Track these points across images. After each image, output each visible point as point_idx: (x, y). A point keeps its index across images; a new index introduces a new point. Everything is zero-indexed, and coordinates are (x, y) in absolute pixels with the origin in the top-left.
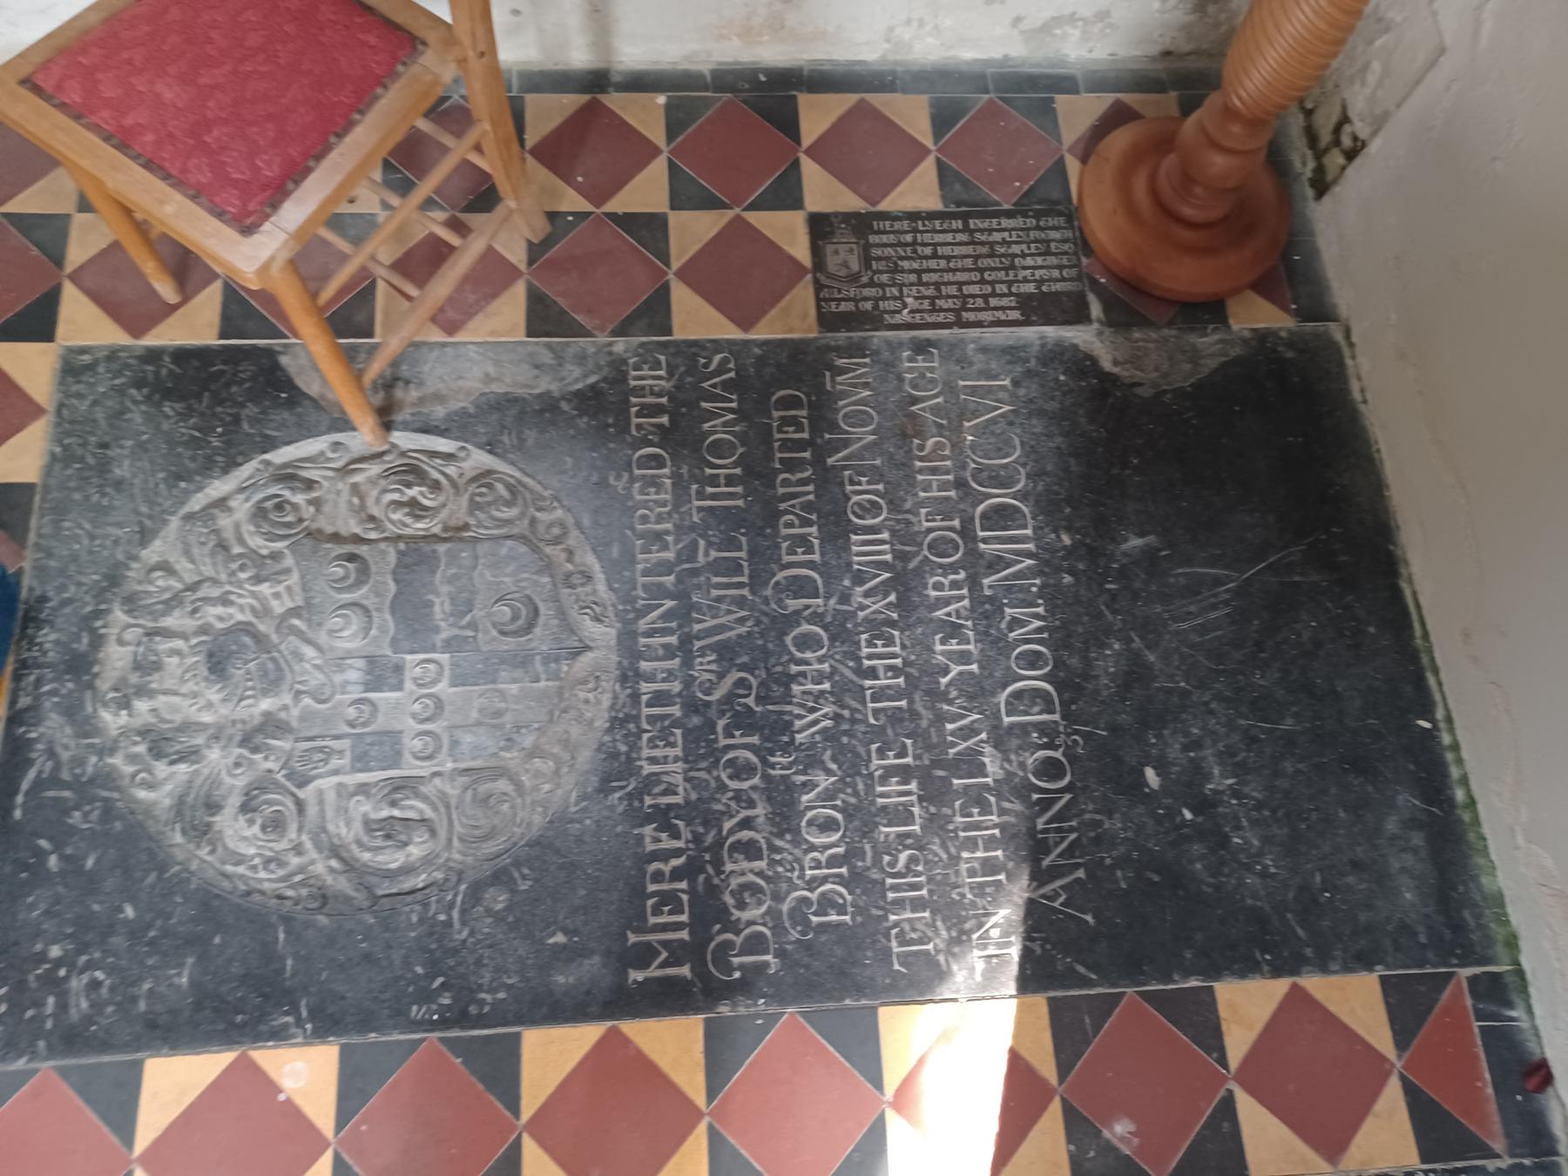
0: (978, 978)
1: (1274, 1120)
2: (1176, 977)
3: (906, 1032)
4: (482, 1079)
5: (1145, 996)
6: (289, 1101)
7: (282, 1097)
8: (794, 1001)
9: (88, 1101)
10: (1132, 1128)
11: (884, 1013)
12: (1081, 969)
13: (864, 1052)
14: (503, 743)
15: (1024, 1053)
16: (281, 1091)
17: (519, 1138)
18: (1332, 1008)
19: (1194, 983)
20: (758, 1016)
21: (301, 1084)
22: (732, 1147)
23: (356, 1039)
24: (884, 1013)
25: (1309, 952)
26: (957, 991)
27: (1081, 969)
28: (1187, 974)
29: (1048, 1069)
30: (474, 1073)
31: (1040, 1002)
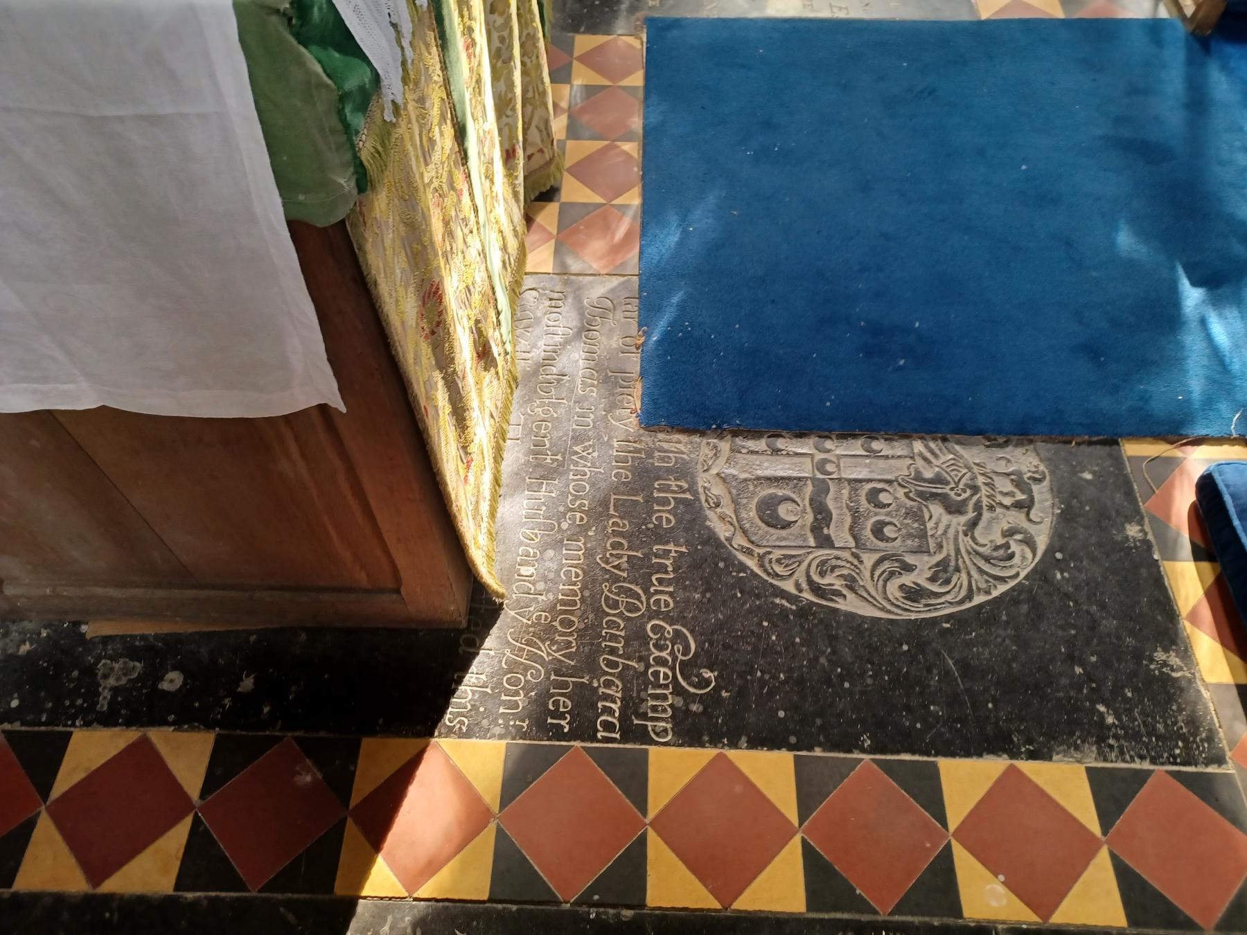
0: (390, 918)
1: (175, 772)
2: (205, 902)
3: (467, 878)
4: (836, 873)
5: (241, 887)
6: (996, 876)
7: (1002, 878)
8: (565, 912)
9: (1161, 895)
10: (297, 778)
11: (367, 744)
12: (291, 918)
13: (510, 866)
14: (999, 510)
15: (368, 847)
16: (1136, 515)
17: (801, 824)
18: (72, 861)
19: (190, 895)
20: (596, 905)
21: (988, 887)
22: (628, 796)
23: (950, 921)
24: (367, 744)
25: (65, 916)
26: (412, 907)
27: (291, 918)
28: (196, 902)
29: (352, 831)
30: (844, 880)
31: (340, 889)
